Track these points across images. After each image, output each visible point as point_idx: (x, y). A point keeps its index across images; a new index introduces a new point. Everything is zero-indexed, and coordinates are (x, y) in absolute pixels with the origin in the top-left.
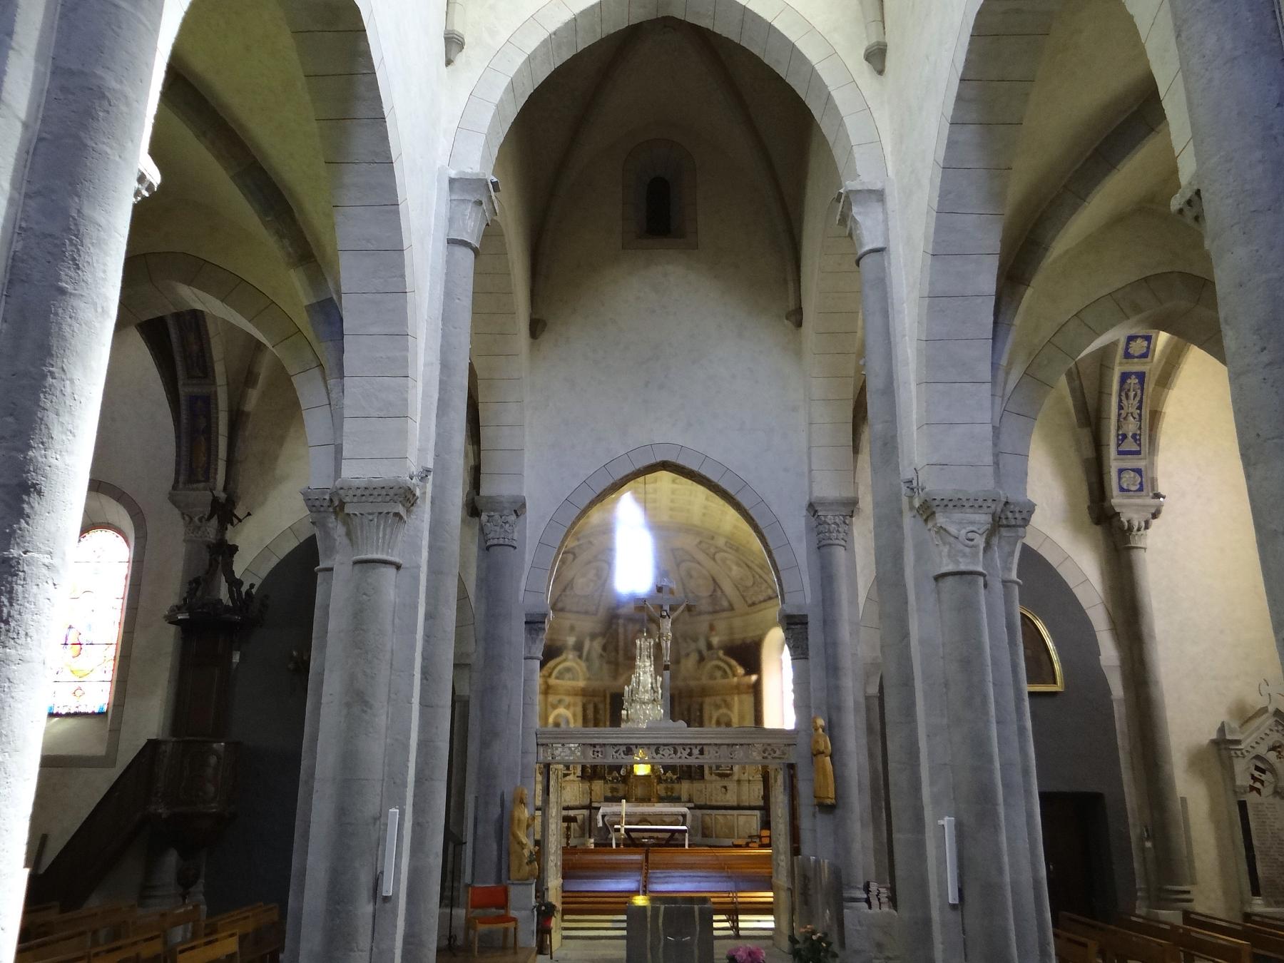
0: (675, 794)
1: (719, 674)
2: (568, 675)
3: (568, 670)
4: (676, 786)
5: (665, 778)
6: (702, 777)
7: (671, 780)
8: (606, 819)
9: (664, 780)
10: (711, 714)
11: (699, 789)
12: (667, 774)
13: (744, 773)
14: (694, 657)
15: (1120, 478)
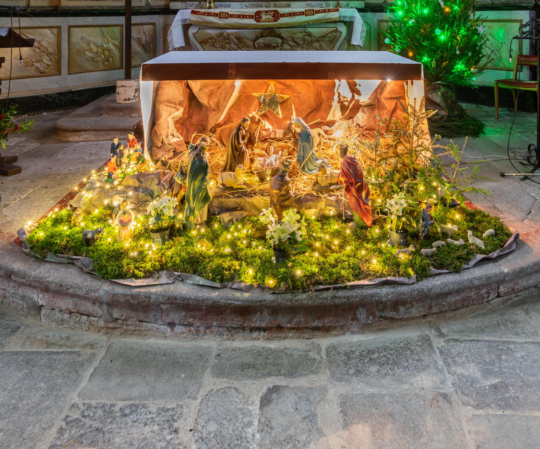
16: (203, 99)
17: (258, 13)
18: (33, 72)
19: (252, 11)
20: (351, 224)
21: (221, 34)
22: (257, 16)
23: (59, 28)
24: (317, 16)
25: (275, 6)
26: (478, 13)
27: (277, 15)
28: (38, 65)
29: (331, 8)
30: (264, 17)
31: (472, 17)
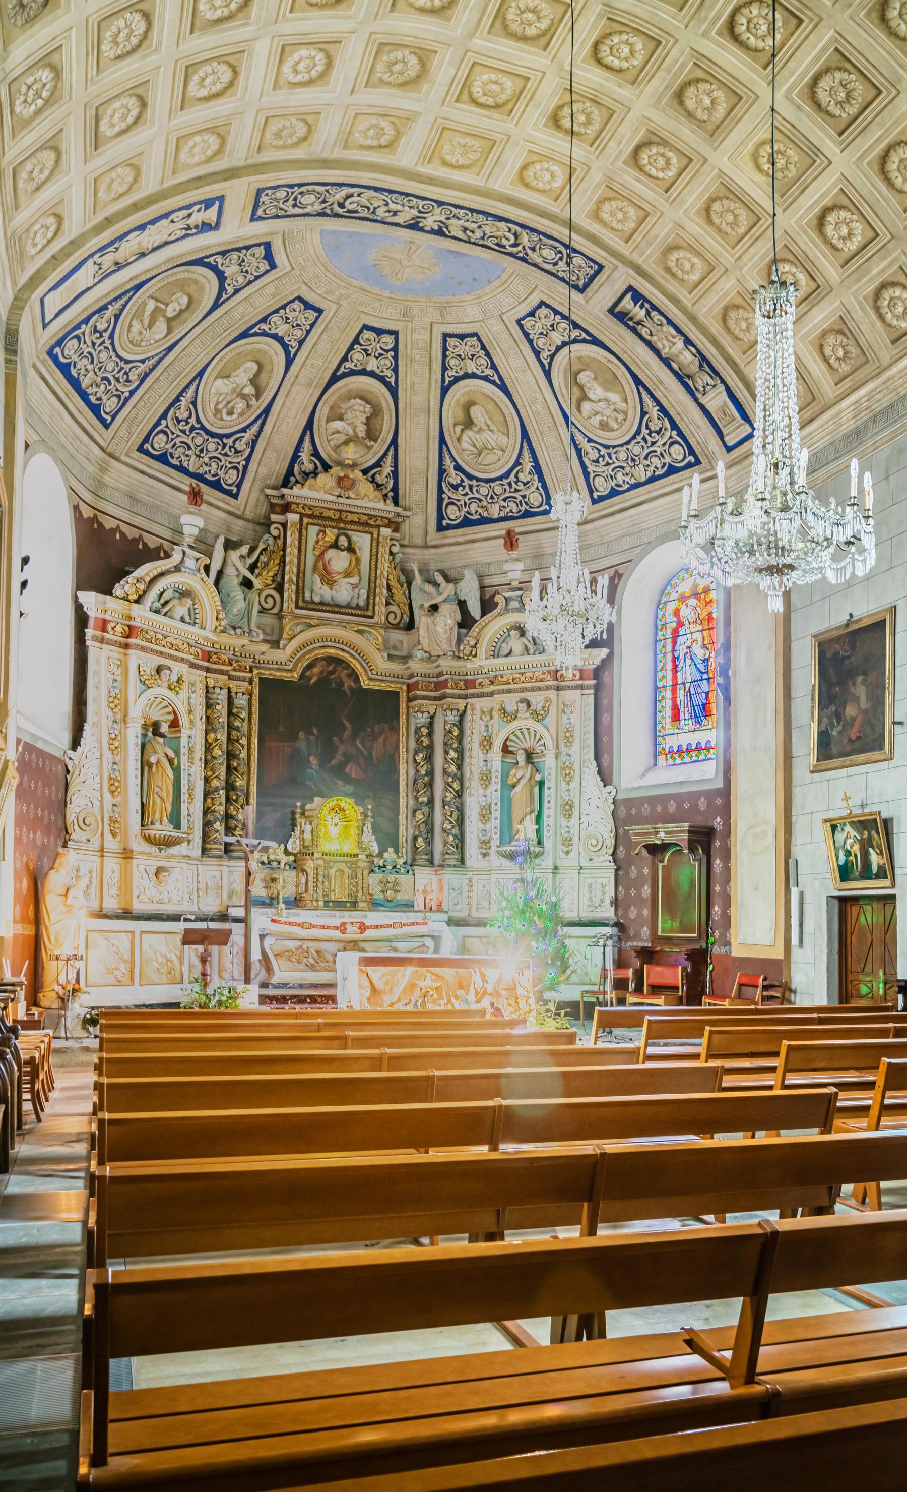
0: (403, 896)
1: (516, 644)
2: (181, 609)
3: (184, 594)
4: (404, 880)
5: (381, 863)
6: (462, 861)
7: (394, 867)
8: (268, 941)
9: (380, 867)
10: (459, 641)
11: (456, 886)
12: (386, 855)
13: (567, 853)
14: (449, 616)
15: (604, 224)
16: (379, 985)
17: (344, 924)
18: (112, 981)
19: (337, 922)
20: (528, 875)
21: (301, 947)
22: (342, 928)
23: (133, 932)
24: (405, 930)
25: (350, 916)
26: (566, 929)
27: (363, 927)
28: (116, 972)
29: (419, 921)
30: (349, 928)
31: (560, 933)
